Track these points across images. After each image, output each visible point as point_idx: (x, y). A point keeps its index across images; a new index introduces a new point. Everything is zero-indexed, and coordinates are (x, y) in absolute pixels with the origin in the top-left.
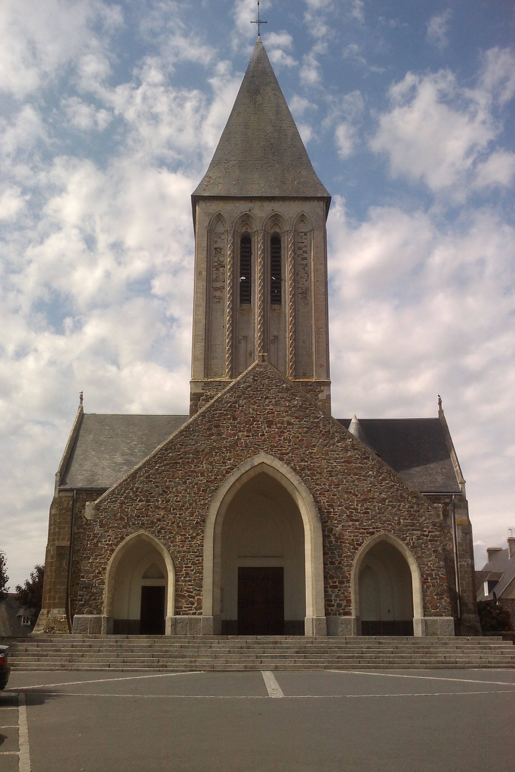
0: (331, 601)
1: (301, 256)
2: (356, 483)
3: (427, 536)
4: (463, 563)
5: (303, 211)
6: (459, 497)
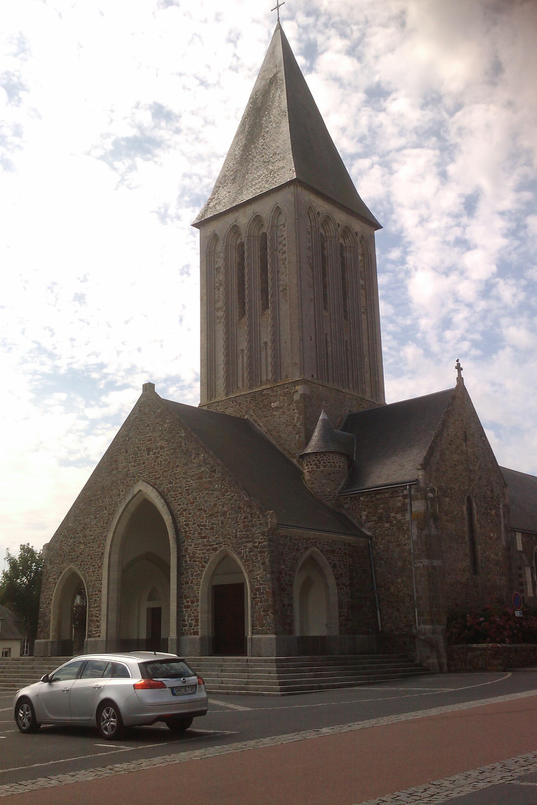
0: (184, 621)
1: (281, 251)
2: (206, 498)
3: (257, 547)
4: (419, 564)
5: (277, 203)
6: (415, 486)
